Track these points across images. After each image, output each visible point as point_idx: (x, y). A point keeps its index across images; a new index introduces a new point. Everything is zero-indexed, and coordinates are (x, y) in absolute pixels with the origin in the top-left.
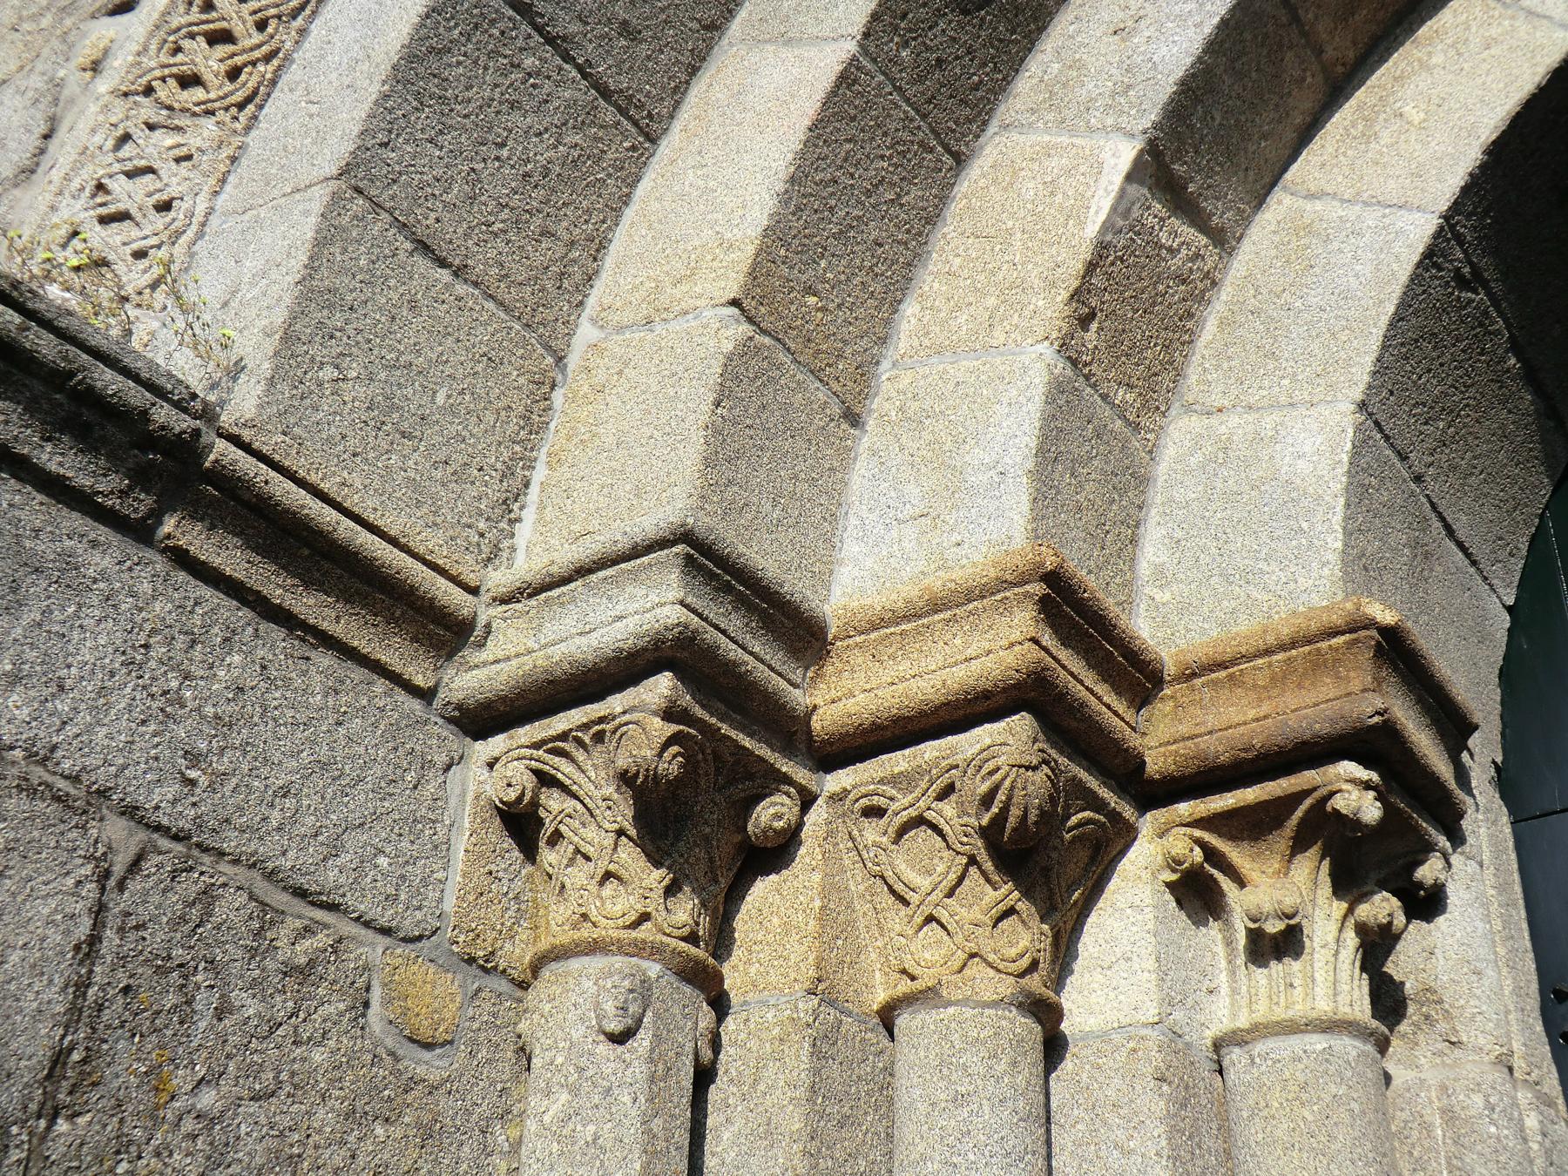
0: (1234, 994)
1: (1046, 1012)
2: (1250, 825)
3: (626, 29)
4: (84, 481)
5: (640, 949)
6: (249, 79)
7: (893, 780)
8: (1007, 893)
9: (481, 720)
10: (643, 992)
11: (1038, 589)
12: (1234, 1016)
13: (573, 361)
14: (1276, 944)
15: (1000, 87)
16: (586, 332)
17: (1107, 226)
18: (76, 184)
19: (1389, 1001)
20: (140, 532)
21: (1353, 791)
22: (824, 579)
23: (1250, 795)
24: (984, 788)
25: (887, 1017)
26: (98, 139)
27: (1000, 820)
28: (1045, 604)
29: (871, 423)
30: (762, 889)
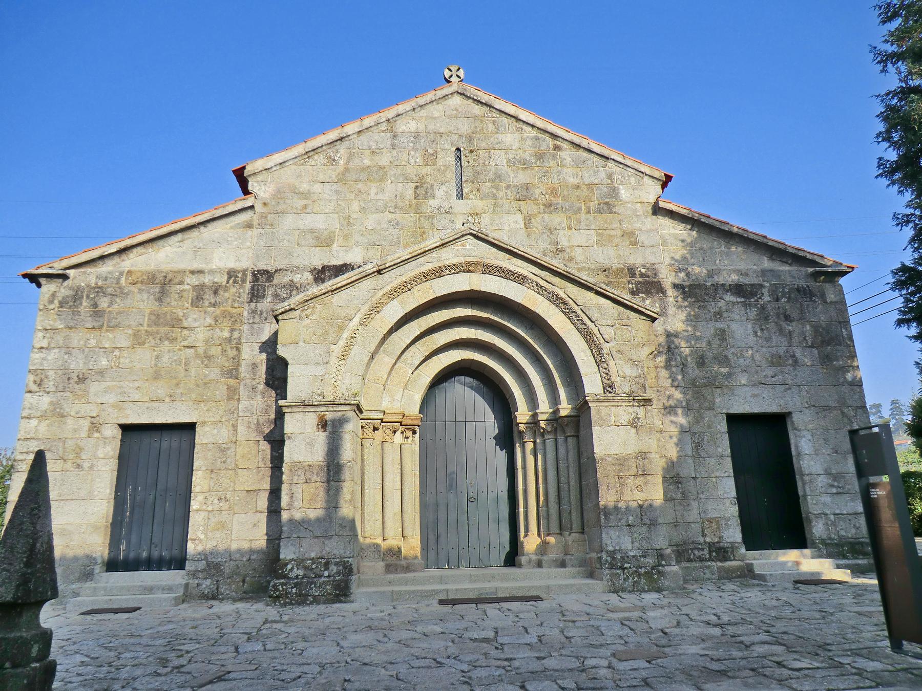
14: (406, 437)
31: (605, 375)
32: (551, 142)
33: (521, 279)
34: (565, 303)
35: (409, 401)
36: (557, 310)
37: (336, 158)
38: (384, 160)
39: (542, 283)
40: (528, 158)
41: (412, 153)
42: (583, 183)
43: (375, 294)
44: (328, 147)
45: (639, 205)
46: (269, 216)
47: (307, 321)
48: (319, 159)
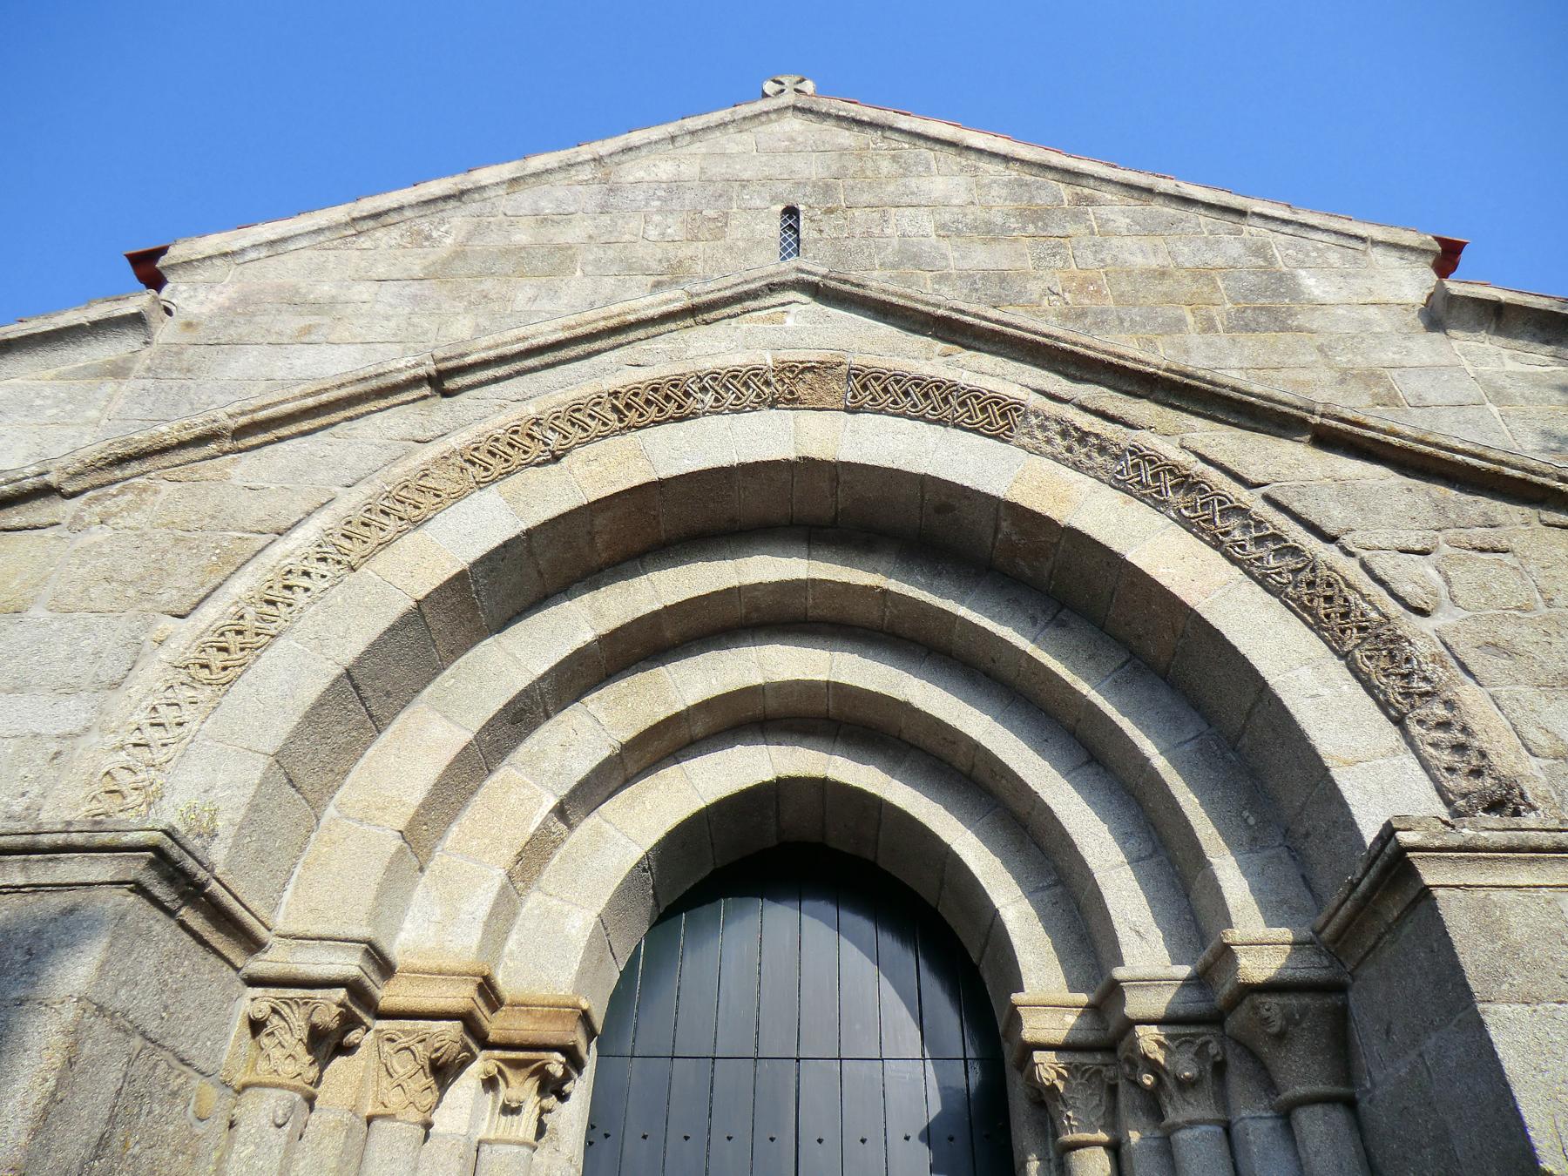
0: (491, 1125)
1: (428, 1126)
2: (517, 1065)
3: (388, 694)
4: (163, 897)
5: (296, 1089)
6: (230, 673)
7: (403, 1032)
8: (431, 1081)
9: (253, 982)
10: (292, 1108)
11: (479, 980)
12: (488, 1130)
13: (323, 822)
14: (510, 1110)
15: (513, 748)
16: (331, 811)
17: (538, 829)
18: (144, 704)
19: (541, 1130)
20: (170, 913)
21: (556, 1064)
22: (393, 936)
23: (521, 1055)
24: (437, 1045)
25: (370, 1120)
26: (158, 684)
27: (438, 1059)
28: (480, 986)
29: (427, 872)
30: (339, 1061)
31: (1447, 757)
32: (1066, 191)
33: (995, 418)
34: (1186, 483)
35: (559, 950)
36: (1159, 520)
37: (435, 234)
38: (573, 234)
39: (1085, 422)
40: (999, 221)
41: (657, 218)
42: (1179, 267)
43: (408, 454)
44: (417, 212)
45: (1372, 309)
46: (191, 350)
47: (99, 534)
48: (385, 238)
